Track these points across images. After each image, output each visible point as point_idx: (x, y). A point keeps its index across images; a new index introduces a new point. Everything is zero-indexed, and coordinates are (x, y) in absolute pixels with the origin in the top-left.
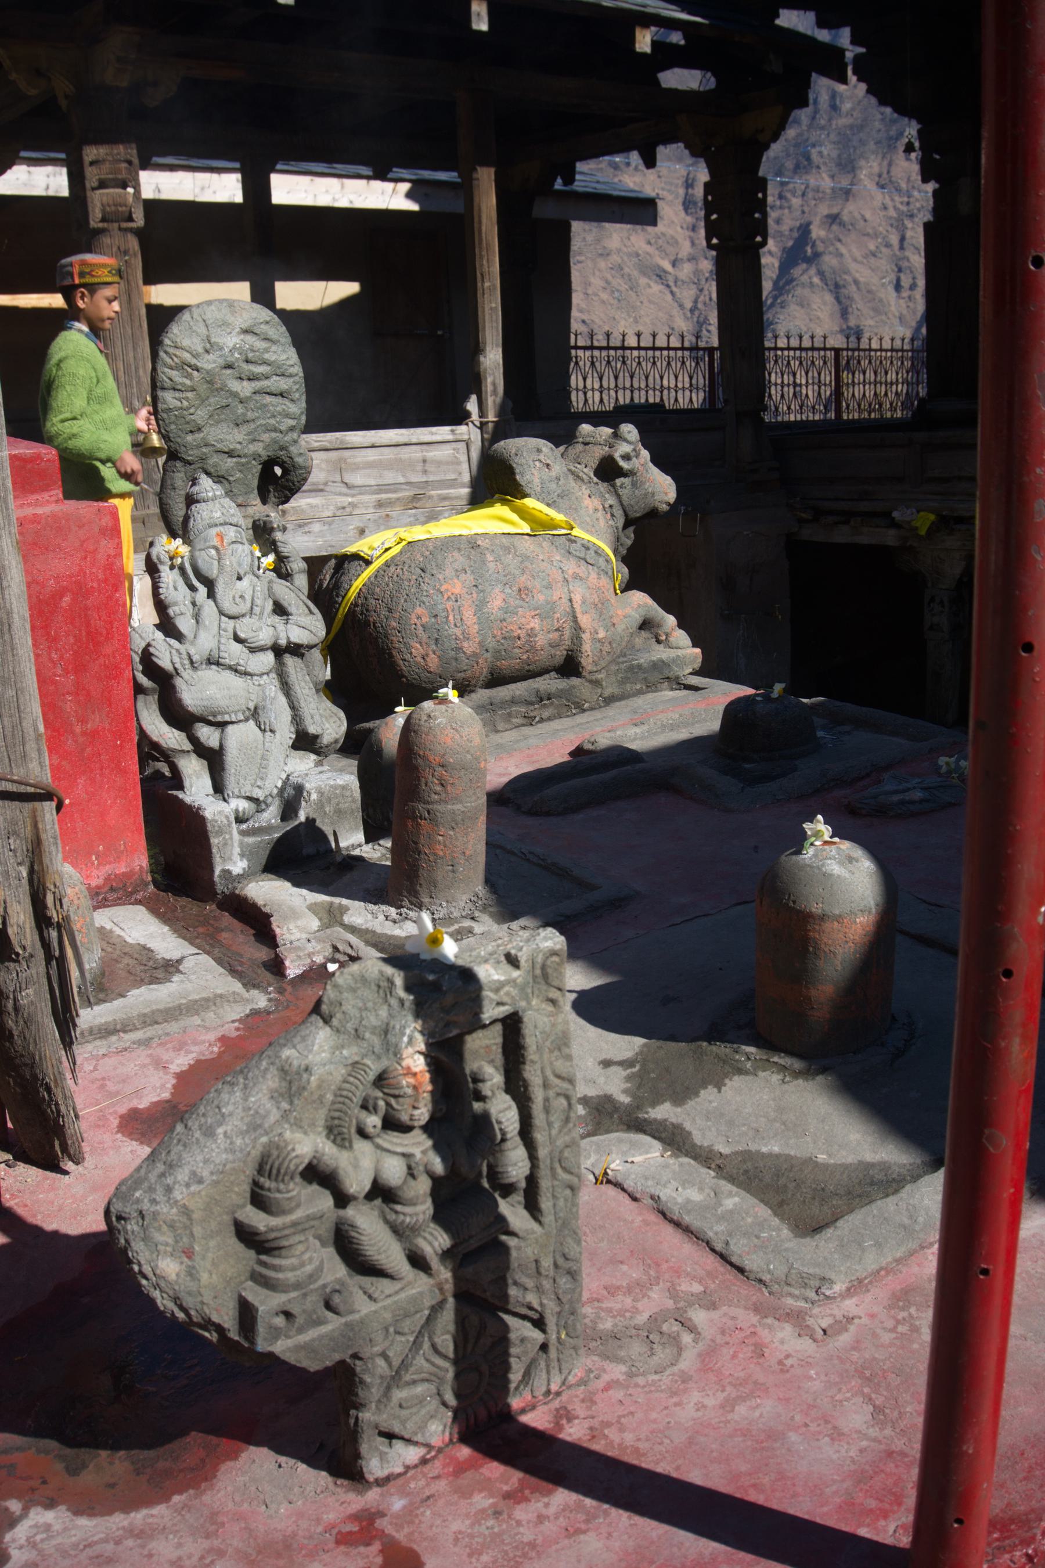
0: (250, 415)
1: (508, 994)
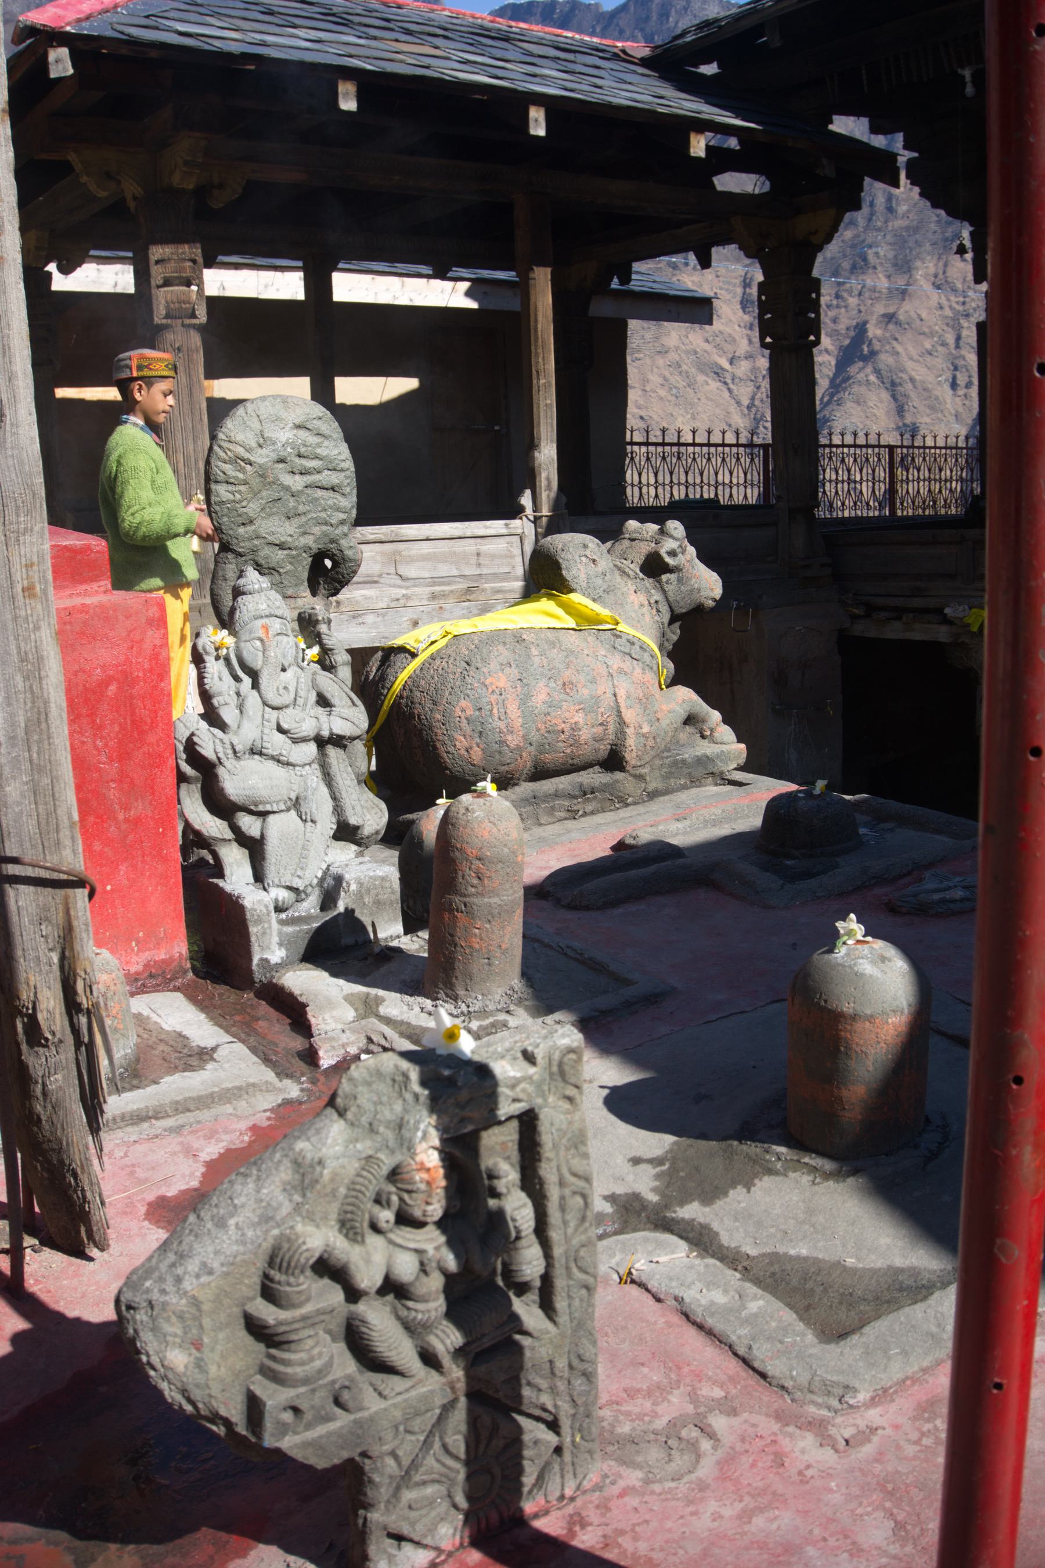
0: (301, 508)
1: (524, 1090)
